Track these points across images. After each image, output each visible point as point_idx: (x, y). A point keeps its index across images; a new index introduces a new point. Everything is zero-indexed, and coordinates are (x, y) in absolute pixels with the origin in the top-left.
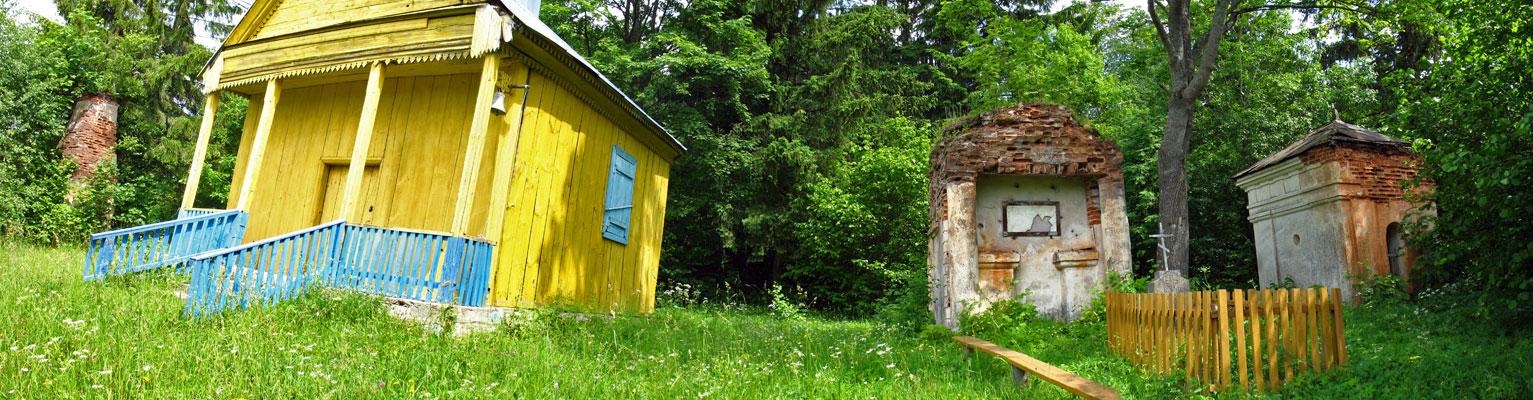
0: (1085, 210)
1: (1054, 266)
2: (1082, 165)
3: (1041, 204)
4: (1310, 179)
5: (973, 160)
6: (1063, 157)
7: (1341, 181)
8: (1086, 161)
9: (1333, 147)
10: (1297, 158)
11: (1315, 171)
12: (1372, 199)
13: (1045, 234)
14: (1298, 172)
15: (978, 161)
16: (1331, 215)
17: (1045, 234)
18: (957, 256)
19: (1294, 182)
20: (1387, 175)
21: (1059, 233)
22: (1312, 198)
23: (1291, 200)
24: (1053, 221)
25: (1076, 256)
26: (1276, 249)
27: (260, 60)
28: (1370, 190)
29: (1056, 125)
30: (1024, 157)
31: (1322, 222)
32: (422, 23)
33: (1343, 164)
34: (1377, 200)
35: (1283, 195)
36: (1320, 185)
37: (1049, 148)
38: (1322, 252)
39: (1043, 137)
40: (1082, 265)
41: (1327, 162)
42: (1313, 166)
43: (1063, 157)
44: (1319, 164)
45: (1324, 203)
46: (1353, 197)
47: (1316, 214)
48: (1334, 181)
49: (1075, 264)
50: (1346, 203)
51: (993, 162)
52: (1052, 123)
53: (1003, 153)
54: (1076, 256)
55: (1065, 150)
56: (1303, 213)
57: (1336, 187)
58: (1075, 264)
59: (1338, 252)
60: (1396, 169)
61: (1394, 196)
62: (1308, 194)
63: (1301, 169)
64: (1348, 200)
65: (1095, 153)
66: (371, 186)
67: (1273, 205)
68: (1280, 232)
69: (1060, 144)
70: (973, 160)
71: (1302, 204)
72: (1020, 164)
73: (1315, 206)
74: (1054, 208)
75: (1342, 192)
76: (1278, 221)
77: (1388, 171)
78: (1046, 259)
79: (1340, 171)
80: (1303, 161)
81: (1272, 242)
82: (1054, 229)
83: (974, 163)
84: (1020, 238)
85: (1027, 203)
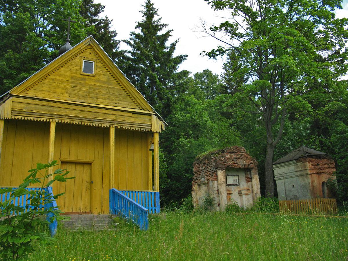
0: (245, 178)
1: (238, 195)
2: (249, 165)
3: (234, 176)
4: (298, 167)
5: (224, 164)
6: (244, 163)
7: (309, 168)
8: (249, 164)
9: (306, 158)
10: (295, 160)
11: (300, 165)
12: (317, 174)
13: (236, 185)
14: (294, 165)
15: (226, 164)
16: (306, 179)
17: (236, 185)
18: (223, 192)
19: (292, 168)
20: (321, 166)
21: (239, 185)
22: (299, 173)
23: (291, 174)
24: (238, 181)
25: (245, 192)
26: (285, 189)
27: (42, 110)
28: (317, 171)
29: (243, 153)
30: (236, 163)
31: (303, 181)
32: (130, 114)
33: (309, 163)
34: (319, 174)
35: (288, 172)
36: (302, 169)
37: (241, 160)
38: (302, 190)
39: (240, 157)
40: (247, 194)
41: (305, 162)
42: (299, 163)
43: (244, 163)
44: (302, 163)
45: (304, 175)
46: (312, 173)
47: (300, 179)
48: (307, 169)
49: (245, 194)
50: (311, 175)
51: (229, 164)
52: (242, 153)
53: (231, 161)
54: (245, 192)
55: (245, 161)
56: (295, 178)
57: (308, 170)
58: (245, 194)
59: (308, 191)
60: (324, 164)
61: (323, 173)
62: (297, 172)
63: (295, 164)
64: (311, 174)
65: (252, 161)
66: (84, 172)
67: (285, 175)
68: (287, 184)
69: (244, 159)
70: (224, 164)
71: (295, 175)
72: (235, 165)
73: (300, 176)
74: (238, 177)
75: (309, 172)
76: (286, 180)
77: (321, 165)
78: (236, 193)
79: (309, 165)
80: (296, 161)
81: (284, 187)
82: (238, 184)
83: (224, 164)
84: (230, 186)
85: (231, 176)
